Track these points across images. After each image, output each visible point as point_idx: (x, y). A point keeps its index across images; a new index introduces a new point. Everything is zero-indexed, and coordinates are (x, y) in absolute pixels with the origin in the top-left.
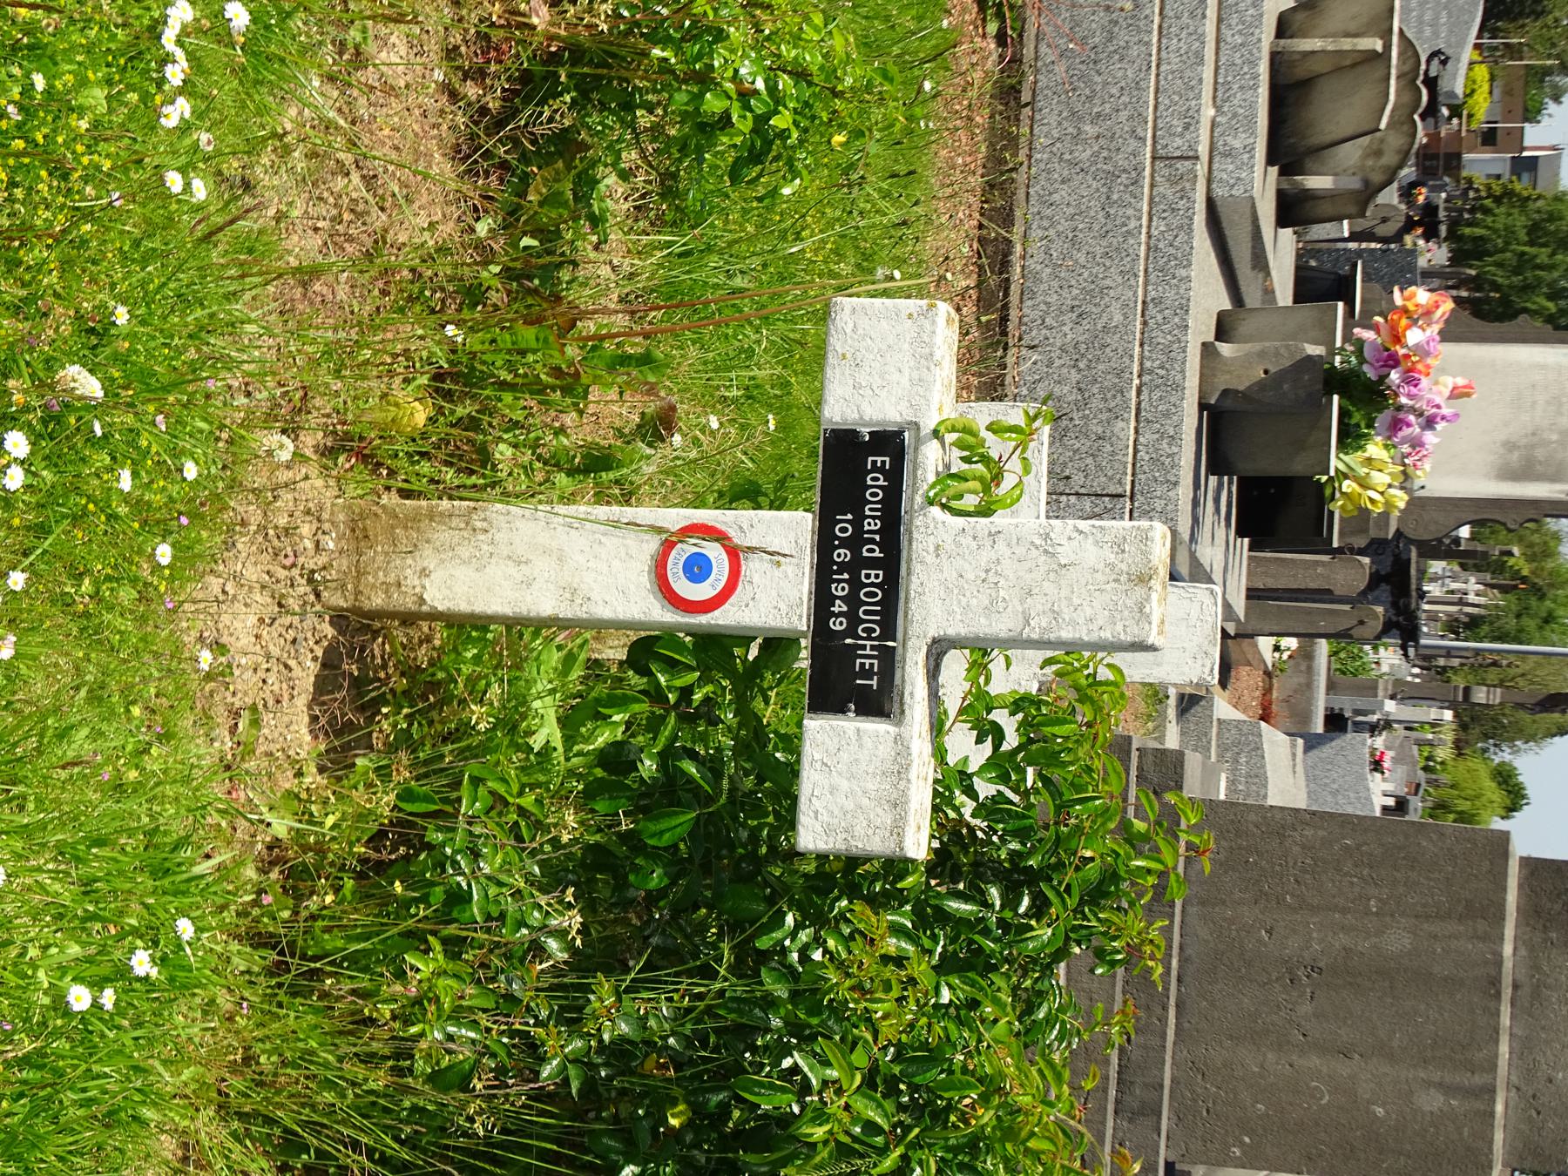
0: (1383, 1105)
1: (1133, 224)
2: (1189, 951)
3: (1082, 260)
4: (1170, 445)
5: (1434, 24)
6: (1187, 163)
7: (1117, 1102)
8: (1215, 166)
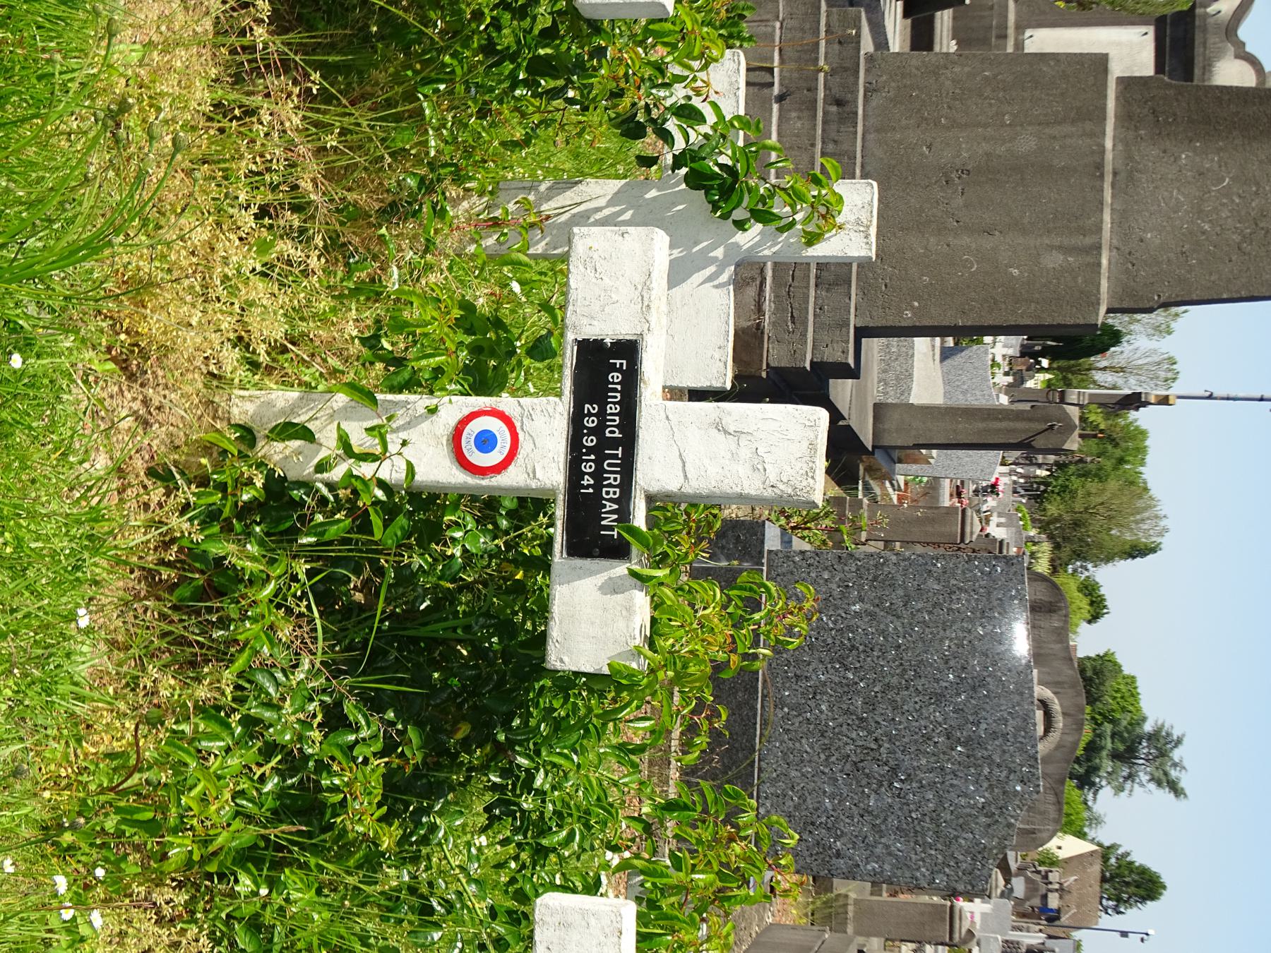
7: (817, 277)
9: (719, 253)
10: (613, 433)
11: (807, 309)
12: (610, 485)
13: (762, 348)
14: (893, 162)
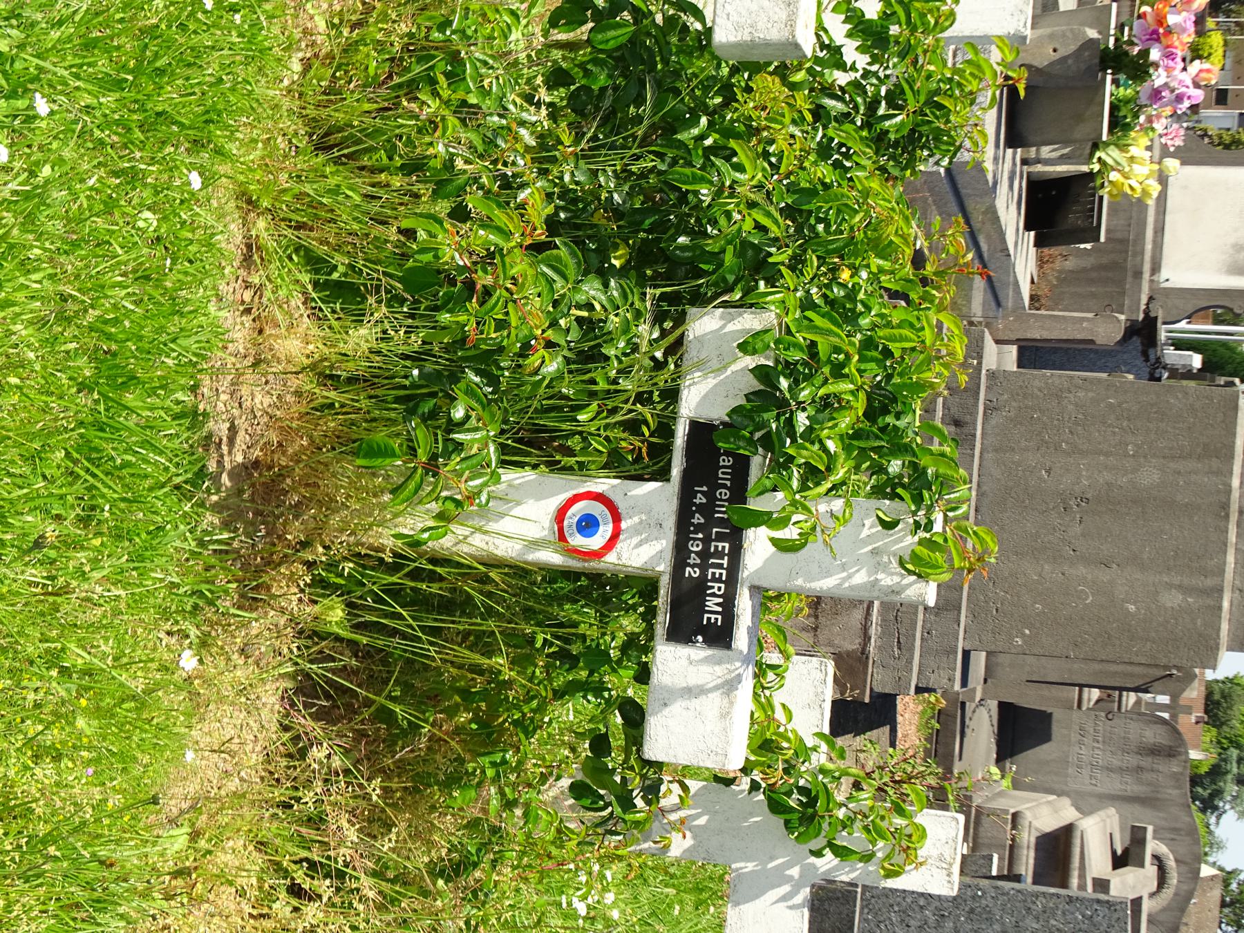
0: (1134, 603)
2: (984, 488)
9: (795, 872)
11: (914, 636)
12: (714, 595)
13: (866, 674)
14: (1011, 484)
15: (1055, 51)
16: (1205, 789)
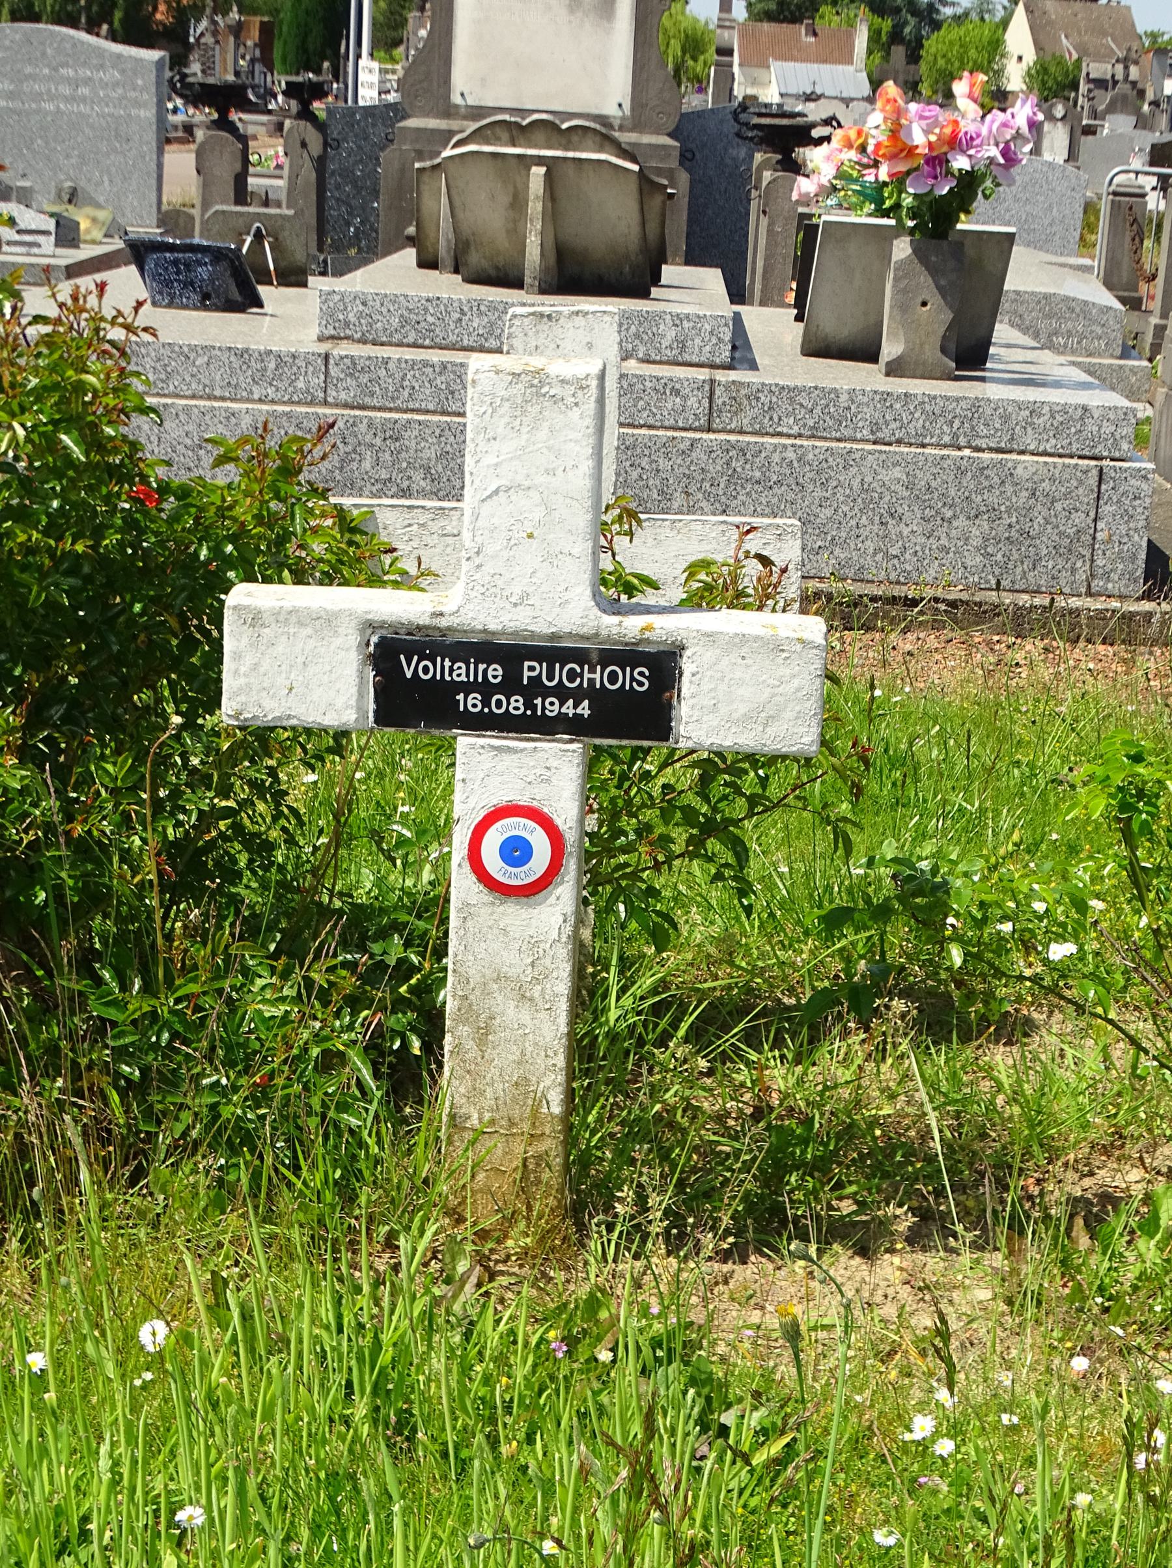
1: (790, 455)
3: (828, 512)
4: (1040, 415)
5: (76, 83)
6: (718, 393)
8: (695, 359)
10: (495, 673)
15: (924, 304)
16: (906, 23)
